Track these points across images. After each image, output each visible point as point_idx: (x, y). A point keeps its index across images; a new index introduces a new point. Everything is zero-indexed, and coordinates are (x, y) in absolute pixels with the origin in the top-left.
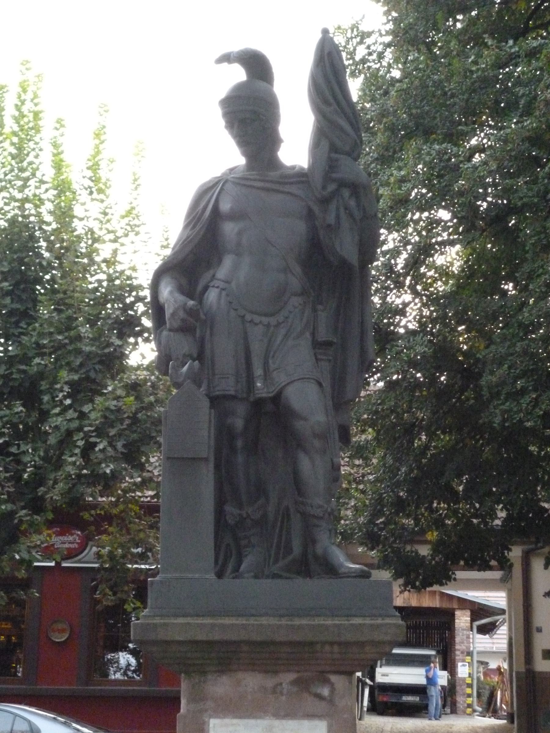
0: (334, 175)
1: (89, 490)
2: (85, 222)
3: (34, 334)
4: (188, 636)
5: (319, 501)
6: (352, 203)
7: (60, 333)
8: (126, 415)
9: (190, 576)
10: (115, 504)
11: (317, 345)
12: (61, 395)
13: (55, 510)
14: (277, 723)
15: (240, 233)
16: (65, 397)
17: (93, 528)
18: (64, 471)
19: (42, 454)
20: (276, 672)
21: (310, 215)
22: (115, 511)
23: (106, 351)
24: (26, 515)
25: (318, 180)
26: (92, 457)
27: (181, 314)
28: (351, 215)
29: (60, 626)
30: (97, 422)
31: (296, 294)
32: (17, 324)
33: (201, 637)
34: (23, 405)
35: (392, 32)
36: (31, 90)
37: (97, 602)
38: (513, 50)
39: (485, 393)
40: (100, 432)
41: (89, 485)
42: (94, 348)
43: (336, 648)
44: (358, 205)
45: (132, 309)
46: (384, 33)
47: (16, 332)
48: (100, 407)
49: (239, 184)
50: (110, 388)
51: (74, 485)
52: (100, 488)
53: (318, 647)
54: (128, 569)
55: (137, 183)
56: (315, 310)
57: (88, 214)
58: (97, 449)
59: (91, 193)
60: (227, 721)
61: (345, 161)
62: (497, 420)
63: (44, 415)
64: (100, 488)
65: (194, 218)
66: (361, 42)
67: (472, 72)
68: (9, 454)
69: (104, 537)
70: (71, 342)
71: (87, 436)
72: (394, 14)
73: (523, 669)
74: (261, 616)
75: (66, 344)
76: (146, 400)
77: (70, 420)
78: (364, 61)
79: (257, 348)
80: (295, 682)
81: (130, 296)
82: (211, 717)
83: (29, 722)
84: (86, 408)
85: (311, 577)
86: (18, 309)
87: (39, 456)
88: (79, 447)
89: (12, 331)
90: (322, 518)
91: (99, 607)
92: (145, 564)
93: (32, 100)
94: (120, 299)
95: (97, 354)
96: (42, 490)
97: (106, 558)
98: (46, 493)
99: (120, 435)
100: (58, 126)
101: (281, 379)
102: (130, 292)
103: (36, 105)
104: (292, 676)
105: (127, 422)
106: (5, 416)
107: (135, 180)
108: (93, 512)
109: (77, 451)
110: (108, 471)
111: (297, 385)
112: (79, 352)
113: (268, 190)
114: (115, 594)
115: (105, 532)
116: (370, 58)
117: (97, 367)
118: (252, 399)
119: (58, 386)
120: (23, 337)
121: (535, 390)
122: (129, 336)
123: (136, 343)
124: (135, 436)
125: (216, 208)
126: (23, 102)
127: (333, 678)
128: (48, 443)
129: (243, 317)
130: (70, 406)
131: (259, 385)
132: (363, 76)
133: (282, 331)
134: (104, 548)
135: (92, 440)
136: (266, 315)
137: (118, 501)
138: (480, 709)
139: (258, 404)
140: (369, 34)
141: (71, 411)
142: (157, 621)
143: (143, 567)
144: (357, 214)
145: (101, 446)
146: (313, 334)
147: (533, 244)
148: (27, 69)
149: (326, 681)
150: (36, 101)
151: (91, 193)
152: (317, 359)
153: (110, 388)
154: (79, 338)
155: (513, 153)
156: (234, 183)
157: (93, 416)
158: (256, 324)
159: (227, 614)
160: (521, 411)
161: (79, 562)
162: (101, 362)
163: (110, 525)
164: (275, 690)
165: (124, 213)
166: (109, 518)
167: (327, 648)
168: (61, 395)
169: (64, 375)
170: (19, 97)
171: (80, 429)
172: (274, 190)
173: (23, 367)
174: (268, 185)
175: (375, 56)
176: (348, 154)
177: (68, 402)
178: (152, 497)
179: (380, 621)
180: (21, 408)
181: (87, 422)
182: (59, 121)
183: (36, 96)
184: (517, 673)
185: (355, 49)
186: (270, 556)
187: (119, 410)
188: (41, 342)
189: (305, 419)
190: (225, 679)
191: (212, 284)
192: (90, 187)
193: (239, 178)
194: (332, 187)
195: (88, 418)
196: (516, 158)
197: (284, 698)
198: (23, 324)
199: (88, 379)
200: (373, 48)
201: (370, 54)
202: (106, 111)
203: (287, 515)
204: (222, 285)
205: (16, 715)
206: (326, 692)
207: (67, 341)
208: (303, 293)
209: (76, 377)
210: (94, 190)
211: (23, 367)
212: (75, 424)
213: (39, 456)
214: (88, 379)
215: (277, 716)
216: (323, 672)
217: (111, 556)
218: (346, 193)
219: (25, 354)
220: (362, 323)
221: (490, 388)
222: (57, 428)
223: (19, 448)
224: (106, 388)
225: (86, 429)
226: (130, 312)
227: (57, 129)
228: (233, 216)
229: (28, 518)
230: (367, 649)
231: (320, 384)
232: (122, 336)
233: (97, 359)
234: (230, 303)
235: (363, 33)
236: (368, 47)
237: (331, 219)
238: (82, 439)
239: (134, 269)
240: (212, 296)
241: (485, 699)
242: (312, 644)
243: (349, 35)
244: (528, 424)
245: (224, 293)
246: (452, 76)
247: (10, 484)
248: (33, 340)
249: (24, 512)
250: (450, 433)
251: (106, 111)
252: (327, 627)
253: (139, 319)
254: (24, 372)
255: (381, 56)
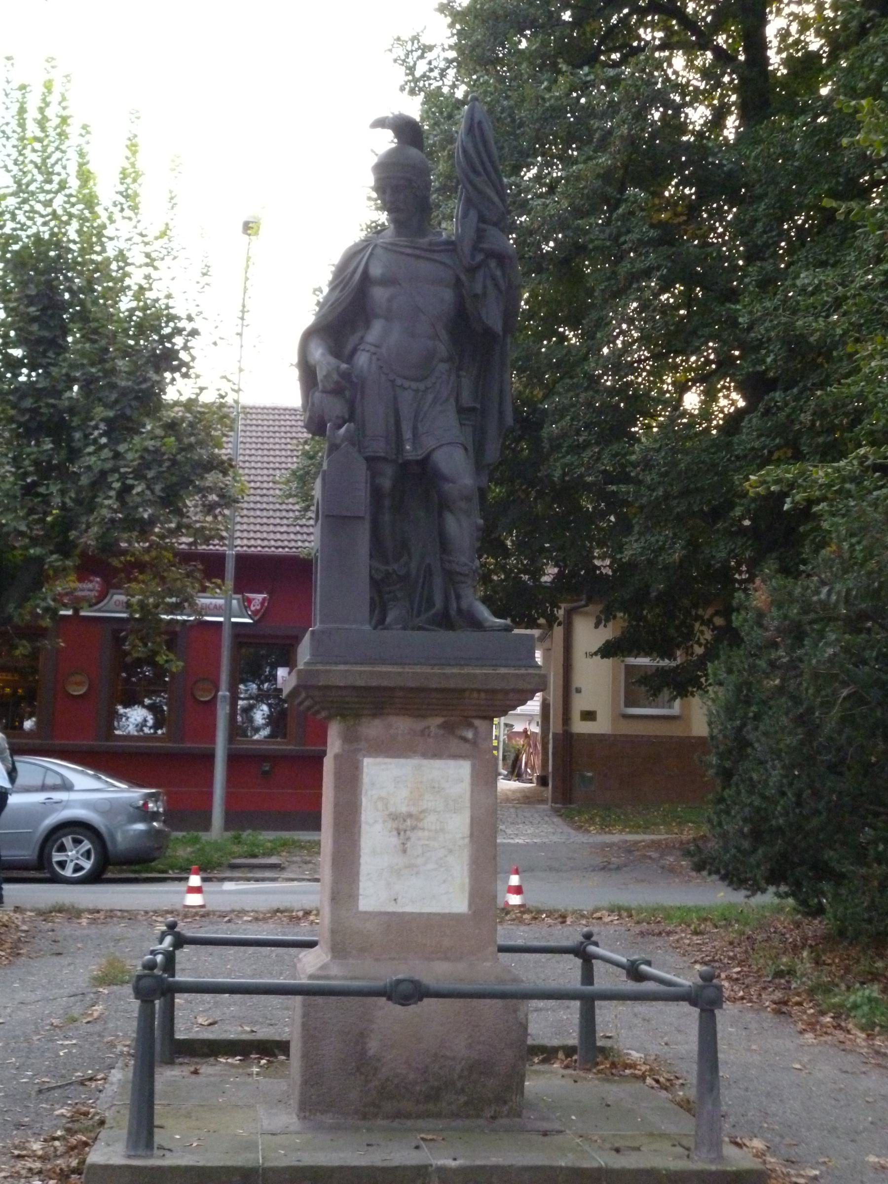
0: (481, 246)
1: (125, 536)
2: (115, 242)
3: (65, 364)
4: (349, 682)
5: (463, 559)
6: (498, 273)
7: (93, 365)
8: (166, 457)
9: (347, 626)
10: (147, 550)
11: (461, 411)
12: (96, 433)
13: (83, 555)
14: (425, 762)
15: (390, 300)
16: (101, 435)
17: (123, 575)
18: (99, 514)
19: (73, 495)
20: (424, 717)
21: (458, 283)
22: (147, 558)
23: (144, 386)
24: (56, 560)
25: (466, 248)
26: (128, 499)
27: (335, 377)
28: (497, 285)
29: (78, 678)
30: (135, 463)
31: (442, 360)
32: (44, 354)
33: (360, 683)
34: (53, 442)
35: (457, 47)
36: (57, 89)
37: (126, 654)
38: (588, 78)
39: (546, 445)
40: (139, 475)
41: (124, 530)
42: (130, 383)
43: (483, 695)
44: (504, 275)
45: (170, 342)
46: (446, 47)
47: (45, 361)
48: (138, 447)
49: (386, 249)
50: (149, 427)
51: (108, 529)
52: (136, 533)
53: (467, 694)
54: (161, 620)
55: (173, 201)
56: (458, 376)
57: (118, 234)
58: (134, 492)
59: (122, 210)
60: (379, 760)
61: (492, 231)
62: (558, 473)
63: (74, 454)
64: (136, 533)
65: (341, 282)
66: (422, 57)
67: (543, 99)
68: (38, 495)
69: (134, 585)
70: (105, 377)
71: (123, 477)
72: (458, 27)
73: (560, 730)
74: (415, 664)
75: (99, 377)
76: (186, 441)
77: (104, 460)
78: (424, 76)
79: (406, 411)
80: (443, 726)
81: (167, 326)
82: (364, 756)
83: (61, 776)
84: (122, 448)
85: (454, 630)
86: (44, 337)
87: (70, 498)
88: (114, 489)
89: (39, 361)
90: (466, 575)
91: (128, 659)
92: (181, 614)
93: (60, 103)
94: (157, 329)
95: (132, 390)
96: (73, 534)
97: (136, 607)
98: (78, 538)
99: (156, 478)
100: (83, 132)
101: (429, 443)
102: (167, 322)
103: (64, 108)
104: (439, 720)
105: (167, 464)
106: (32, 453)
107: (172, 198)
108: (122, 558)
109: (112, 493)
110: (146, 516)
111: (445, 449)
112: (113, 386)
113: (418, 257)
114: (145, 645)
115: (136, 580)
116: (432, 75)
117: (134, 403)
118: (400, 461)
119: (93, 423)
120: (52, 368)
121: (597, 443)
122: (166, 371)
123: (173, 379)
124: (174, 479)
125: (365, 273)
126: (47, 104)
127: (477, 722)
128: (80, 483)
129: (393, 381)
130: (105, 446)
131: (408, 447)
132: (422, 94)
133: (430, 397)
134: (133, 596)
135: (130, 482)
136: (415, 380)
137: (151, 546)
138: (505, 773)
139: (406, 464)
140: (431, 48)
141: (106, 451)
142: (320, 667)
143: (179, 618)
144: (503, 286)
145: (139, 489)
146: (457, 401)
147: (603, 291)
148: (53, 67)
149: (470, 725)
150: (63, 104)
151: (122, 210)
152: (461, 424)
153: (149, 427)
154: (113, 371)
155: (586, 191)
156: (382, 247)
157: (130, 456)
158: (405, 389)
159: (383, 662)
160: (582, 464)
161: (99, 611)
162: (137, 398)
163: (141, 572)
164: (424, 733)
165: (158, 234)
166: (141, 566)
167: (475, 695)
168: (96, 433)
169: (100, 412)
170: (44, 100)
171: (115, 470)
172: (423, 258)
173: (52, 401)
174: (418, 252)
175: (436, 73)
176: (495, 224)
177: (104, 440)
178: (190, 544)
179: (523, 671)
180: (51, 446)
181: (122, 463)
182: (84, 127)
183: (64, 99)
184: (555, 735)
185: (415, 64)
186: (412, 609)
187: (157, 451)
188: (72, 374)
189: (454, 482)
190: (377, 722)
191: (362, 347)
192: (121, 204)
193: (391, 244)
194: (480, 257)
195: (124, 459)
196: (588, 198)
197: (431, 740)
198: (50, 354)
199: (123, 416)
200: (434, 63)
201: (431, 70)
202: (138, 118)
203: (429, 571)
204: (373, 349)
205: (48, 769)
206: (470, 735)
207: (100, 374)
208: (450, 359)
209: (111, 414)
210: (125, 206)
211: (52, 401)
212: (109, 465)
213: (70, 498)
214: (123, 416)
215: (425, 755)
216: (467, 717)
217: (142, 606)
218: (493, 264)
219: (54, 386)
220: (501, 391)
221: (550, 440)
222: (89, 468)
223: (47, 489)
224: (144, 426)
225: (122, 470)
226: (168, 345)
227: (81, 135)
228: (387, 281)
229: (59, 563)
230: (511, 695)
231: (466, 449)
232: (159, 370)
233: (134, 395)
234: (381, 367)
235: (425, 46)
236: (430, 63)
237: (478, 289)
238: (118, 481)
239: (169, 296)
240: (362, 359)
241: (510, 762)
242: (464, 690)
243: (409, 48)
244: (590, 479)
245: (374, 358)
246: (523, 101)
247: (38, 527)
248: (64, 371)
249: (55, 556)
250: (501, 484)
251: (138, 118)
252: (475, 675)
253: (177, 352)
254: (53, 406)
255: (443, 75)
